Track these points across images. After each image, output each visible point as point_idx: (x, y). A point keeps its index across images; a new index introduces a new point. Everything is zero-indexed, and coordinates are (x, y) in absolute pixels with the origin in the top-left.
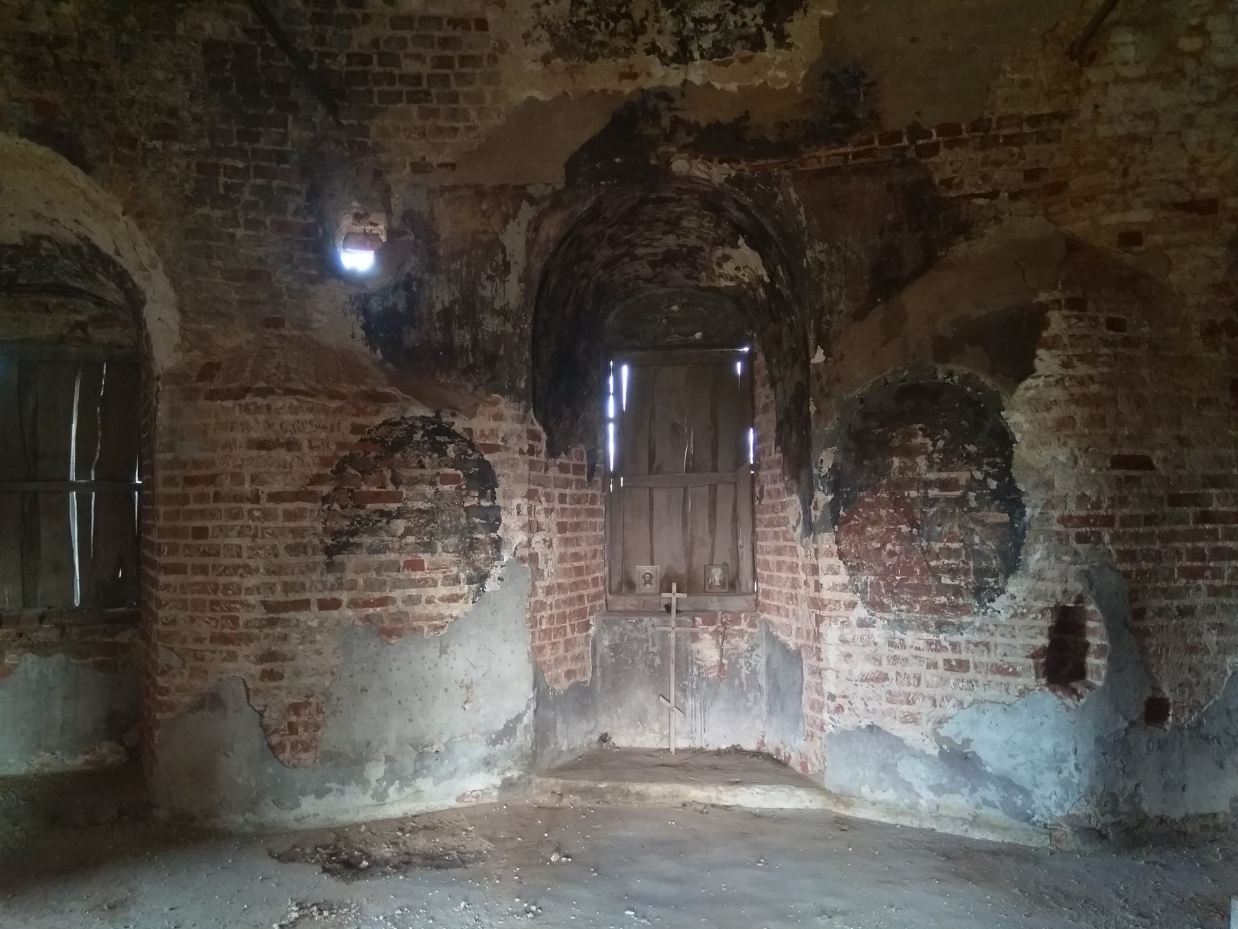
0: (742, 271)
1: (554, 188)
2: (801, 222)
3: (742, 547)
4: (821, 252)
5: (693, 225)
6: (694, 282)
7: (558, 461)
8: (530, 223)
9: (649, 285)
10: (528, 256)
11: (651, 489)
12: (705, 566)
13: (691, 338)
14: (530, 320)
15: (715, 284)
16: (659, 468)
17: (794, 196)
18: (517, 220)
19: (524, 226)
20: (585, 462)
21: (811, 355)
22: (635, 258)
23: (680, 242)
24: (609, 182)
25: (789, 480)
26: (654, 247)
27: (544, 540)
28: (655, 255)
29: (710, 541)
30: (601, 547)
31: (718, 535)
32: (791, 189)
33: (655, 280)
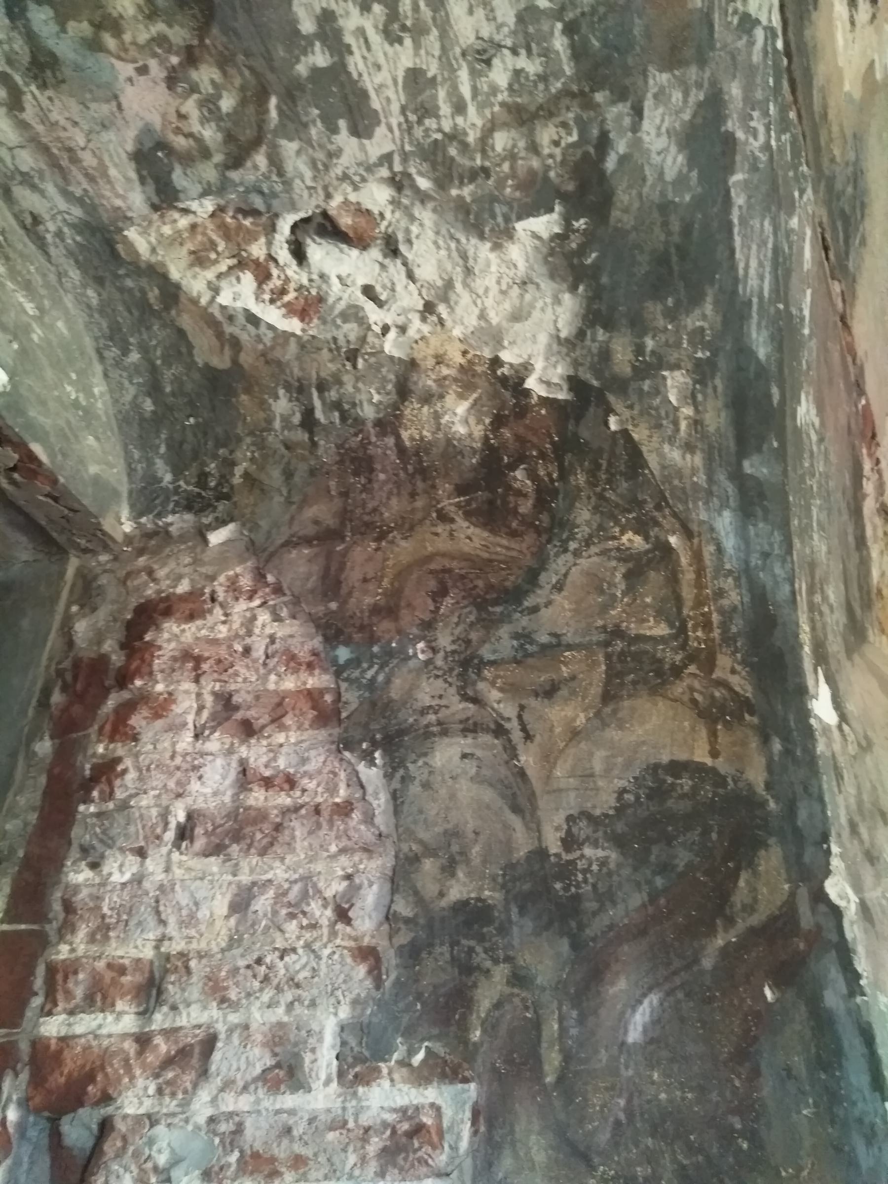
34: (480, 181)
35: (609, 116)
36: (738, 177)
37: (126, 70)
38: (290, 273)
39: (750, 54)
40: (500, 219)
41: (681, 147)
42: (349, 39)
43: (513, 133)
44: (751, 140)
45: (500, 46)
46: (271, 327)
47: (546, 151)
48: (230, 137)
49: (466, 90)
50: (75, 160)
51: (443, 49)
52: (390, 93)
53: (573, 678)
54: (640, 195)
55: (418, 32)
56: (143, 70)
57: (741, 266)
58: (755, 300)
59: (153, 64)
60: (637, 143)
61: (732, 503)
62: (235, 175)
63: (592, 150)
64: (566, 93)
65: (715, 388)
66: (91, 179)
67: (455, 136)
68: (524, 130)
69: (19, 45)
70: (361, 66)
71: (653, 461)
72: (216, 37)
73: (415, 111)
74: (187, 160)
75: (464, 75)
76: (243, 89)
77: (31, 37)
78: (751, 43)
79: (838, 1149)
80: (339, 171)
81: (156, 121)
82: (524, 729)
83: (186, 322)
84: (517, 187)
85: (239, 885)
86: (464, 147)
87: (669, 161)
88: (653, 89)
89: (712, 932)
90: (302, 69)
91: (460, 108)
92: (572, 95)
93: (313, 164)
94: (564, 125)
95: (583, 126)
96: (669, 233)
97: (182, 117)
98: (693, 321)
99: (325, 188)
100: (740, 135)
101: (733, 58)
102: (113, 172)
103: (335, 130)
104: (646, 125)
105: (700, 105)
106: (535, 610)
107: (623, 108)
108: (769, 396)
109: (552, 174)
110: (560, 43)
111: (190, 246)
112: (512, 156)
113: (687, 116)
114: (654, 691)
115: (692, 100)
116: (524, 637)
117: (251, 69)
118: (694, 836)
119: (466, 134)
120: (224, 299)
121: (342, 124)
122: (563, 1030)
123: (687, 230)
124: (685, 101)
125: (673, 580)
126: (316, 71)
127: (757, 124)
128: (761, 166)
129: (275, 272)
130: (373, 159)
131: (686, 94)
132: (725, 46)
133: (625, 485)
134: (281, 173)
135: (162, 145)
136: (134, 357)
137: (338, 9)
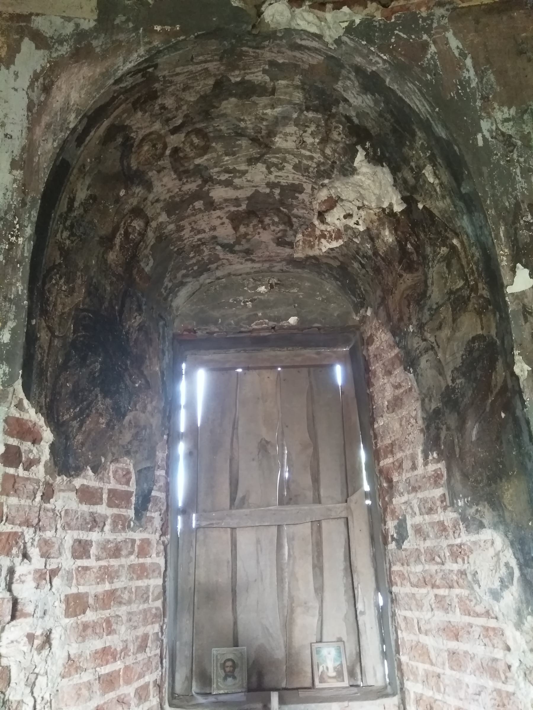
0: (355, 219)
1: (77, 25)
2: (469, 81)
3: (363, 613)
4: (506, 120)
5: (290, 144)
6: (287, 251)
7: (78, 482)
8: (36, 77)
9: (230, 256)
10: (30, 130)
11: (233, 529)
12: (311, 644)
13: (284, 323)
14: (29, 231)
15: (315, 252)
16: (243, 499)
17: (454, 43)
18: (13, 68)
19: (24, 82)
20: (132, 487)
21: (506, 279)
22: (211, 205)
23: (272, 178)
24: (168, 28)
25: (469, 505)
26: (236, 188)
27: (31, 637)
28: (237, 201)
29: (317, 605)
30: (156, 628)
31: (327, 595)
32: (450, 35)
33: (237, 248)
34: (335, 166)
35: (342, 111)
36: (388, 80)
37: (257, 237)
38: (328, 229)
39: (349, 46)
40: (349, 169)
41: (366, 94)
42: (276, 181)
43: (328, 146)
44: (378, 65)
45: (301, 136)
46: (336, 248)
47: (340, 139)
48: (285, 223)
49: (308, 153)
50: (271, 257)
51: (292, 154)
52: (297, 176)
53: (445, 318)
54: (372, 119)
55: (284, 160)
56: (259, 233)
57: (415, 107)
58: (428, 116)
59: (259, 230)
60: (355, 108)
61: (465, 211)
62: (294, 228)
63: (349, 124)
64: (326, 121)
65: (439, 163)
66: (278, 256)
67: (319, 164)
68: (329, 141)
69: (241, 254)
70: (285, 181)
71: (436, 212)
72: (260, 214)
73: (305, 172)
74: (285, 235)
75: (303, 151)
76: (275, 214)
77: (240, 251)
78: (346, 43)
79: (522, 464)
80: (308, 203)
81: (272, 237)
82: (437, 345)
83: (325, 260)
84: (344, 157)
85: (36, 571)
86: (323, 164)
87: (367, 101)
88: (341, 90)
89: (488, 399)
90: (277, 197)
91: (311, 158)
92: (328, 119)
93: (303, 208)
94: (336, 127)
95: (340, 122)
96: (389, 121)
97: (274, 231)
98: (419, 143)
99: (310, 209)
100: (374, 69)
101: (347, 53)
102: (278, 251)
103: (297, 198)
104: (351, 100)
105: (356, 76)
106: (430, 296)
107: (342, 104)
108: (455, 151)
109: (347, 142)
110: (310, 115)
111: (307, 246)
112: (334, 151)
113: (357, 84)
114: (465, 312)
115: (353, 78)
116: (430, 309)
117: (271, 209)
118: (480, 364)
119: (320, 161)
120: (324, 250)
121: (297, 195)
122: (458, 441)
123: (393, 115)
124: (352, 81)
125: (459, 259)
126: (280, 194)
127: (375, 59)
128: (389, 69)
129: (326, 233)
130: (311, 192)
131: (350, 79)
132: (342, 55)
133: (433, 228)
134: (300, 217)
135: (278, 239)
136: (327, 275)
137: (268, 180)
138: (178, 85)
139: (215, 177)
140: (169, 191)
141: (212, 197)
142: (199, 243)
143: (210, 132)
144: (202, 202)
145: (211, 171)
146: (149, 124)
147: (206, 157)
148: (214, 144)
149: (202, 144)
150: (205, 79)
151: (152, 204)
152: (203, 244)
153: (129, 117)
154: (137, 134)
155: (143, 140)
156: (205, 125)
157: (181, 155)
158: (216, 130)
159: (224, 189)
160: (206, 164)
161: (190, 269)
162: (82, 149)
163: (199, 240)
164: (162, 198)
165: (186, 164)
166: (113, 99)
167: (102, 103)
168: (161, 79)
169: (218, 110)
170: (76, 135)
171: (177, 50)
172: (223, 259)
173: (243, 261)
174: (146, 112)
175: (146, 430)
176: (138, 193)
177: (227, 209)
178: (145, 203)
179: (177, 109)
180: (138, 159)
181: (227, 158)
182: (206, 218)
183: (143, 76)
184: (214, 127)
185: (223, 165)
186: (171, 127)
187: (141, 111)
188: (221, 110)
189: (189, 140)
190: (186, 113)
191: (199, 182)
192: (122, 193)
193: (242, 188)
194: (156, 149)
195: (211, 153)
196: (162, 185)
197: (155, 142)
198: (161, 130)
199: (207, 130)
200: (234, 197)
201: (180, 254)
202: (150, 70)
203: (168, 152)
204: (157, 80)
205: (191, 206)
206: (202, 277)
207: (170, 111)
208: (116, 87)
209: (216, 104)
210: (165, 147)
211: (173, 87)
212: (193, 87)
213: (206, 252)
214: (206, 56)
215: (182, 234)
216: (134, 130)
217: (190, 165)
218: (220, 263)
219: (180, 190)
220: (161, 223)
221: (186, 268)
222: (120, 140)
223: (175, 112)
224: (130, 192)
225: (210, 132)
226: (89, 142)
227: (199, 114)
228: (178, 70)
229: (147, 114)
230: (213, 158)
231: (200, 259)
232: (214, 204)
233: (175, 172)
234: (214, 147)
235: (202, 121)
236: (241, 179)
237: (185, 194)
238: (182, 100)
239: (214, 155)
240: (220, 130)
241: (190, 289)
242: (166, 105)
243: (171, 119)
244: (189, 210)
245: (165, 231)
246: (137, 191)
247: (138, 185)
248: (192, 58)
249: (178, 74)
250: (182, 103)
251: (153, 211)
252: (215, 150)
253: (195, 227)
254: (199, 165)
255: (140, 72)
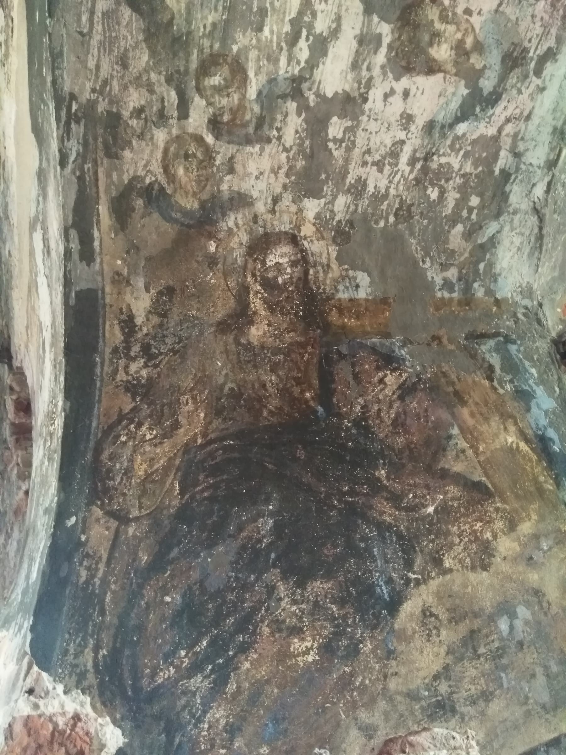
26: (335, 33)
37: (476, 21)
56: (468, 12)
69: (513, 79)
77: (503, 78)
138: (115, 73)
139: (296, 72)
140: (275, 171)
141: (336, 93)
142: (418, 166)
143: (211, 47)
144: (335, 119)
145: (281, 72)
146: (150, 147)
147: (251, 74)
148: (235, 48)
149: (226, 70)
150: (119, 24)
151: (273, 212)
152: (428, 157)
153: (121, 173)
154: (152, 173)
155: (166, 170)
156: (195, 51)
157: (226, 118)
158: (211, 33)
159: (329, 59)
160: (263, 78)
161: (465, 213)
162: (98, 260)
163: (412, 162)
164: (278, 190)
165: (248, 117)
166: (81, 179)
167: (73, 196)
168: (94, 96)
169: (177, 16)
170: (76, 256)
171: (61, 54)
172: (500, 131)
173: (537, 81)
174: (130, 142)
175: (513, 616)
176: (237, 225)
177: (377, 71)
178: (260, 223)
179: (151, 91)
180: (187, 193)
181: (266, 31)
182: (373, 126)
183: (78, 122)
184: (204, 35)
185: (278, 44)
186: (175, 114)
187: (123, 149)
188: (180, 11)
189: (209, 93)
190: (163, 79)
191: (292, 106)
192: (212, 247)
193: (338, 19)
194: (194, 155)
195: (247, 59)
196: (257, 178)
197: (182, 153)
198: (169, 133)
199: (207, 51)
200: (355, 44)
201: (411, 216)
202: (74, 107)
203: (210, 139)
204: (92, 104)
205: (331, 145)
206: (513, 199)
207: (150, 104)
208: (70, 167)
209: (166, 18)
210: (199, 140)
211: (115, 83)
212: (126, 50)
213: (455, 161)
214: (83, 9)
215: (371, 189)
216: (143, 174)
217: (252, 110)
218: (506, 142)
219: (286, 150)
220: (318, 216)
221: (454, 220)
222: (139, 203)
223: (154, 97)
224: (222, 235)
225: (211, 47)
226: (101, 245)
227: (175, 55)
228: (91, 64)
229: (134, 142)
230: (258, 60)
231: (459, 181)
232: (352, 95)
233: (248, 141)
234: (239, 50)
235: (188, 55)
236: (319, 15)
237: (301, 145)
238: (139, 78)
239: (253, 54)
240: (214, 25)
241: (517, 241)
242: (137, 105)
243: (163, 107)
244: (336, 153)
245: (337, 218)
246: (231, 224)
247: (224, 215)
248: (81, 33)
249: (98, 67)
250: (145, 78)
251: (286, 218)
252: (246, 49)
253: (377, 157)
254: (260, 93)
255: (70, 124)
